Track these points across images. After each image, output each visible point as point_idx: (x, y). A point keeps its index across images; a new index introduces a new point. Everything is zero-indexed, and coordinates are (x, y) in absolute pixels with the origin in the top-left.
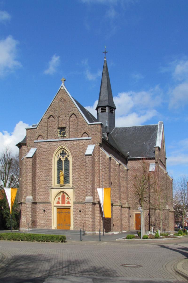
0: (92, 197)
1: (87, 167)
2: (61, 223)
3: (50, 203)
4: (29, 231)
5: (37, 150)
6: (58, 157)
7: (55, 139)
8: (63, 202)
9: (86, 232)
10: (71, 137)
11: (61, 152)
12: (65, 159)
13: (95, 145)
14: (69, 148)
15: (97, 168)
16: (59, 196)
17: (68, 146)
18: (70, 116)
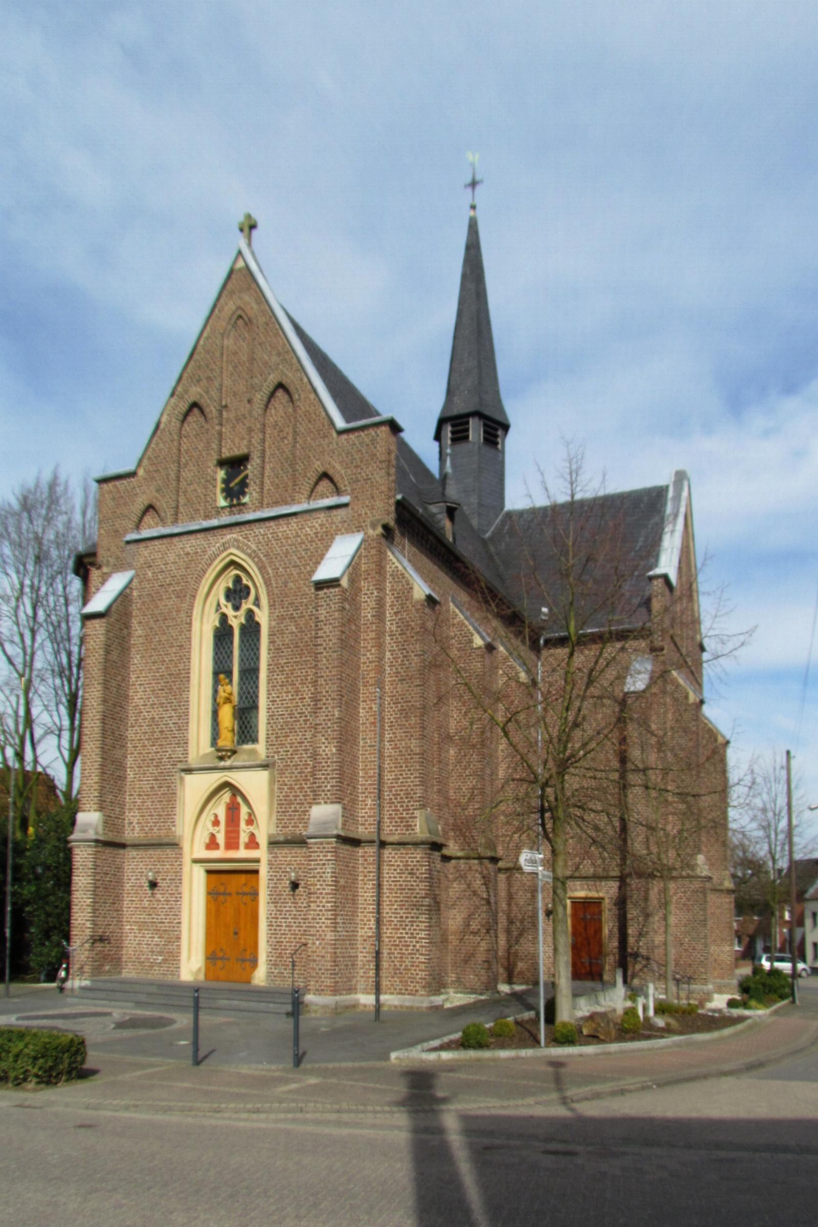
0: (336, 808)
1: (320, 649)
2: (222, 950)
3: (175, 845)
4: (76, 993)
5: (135, 580)
6: (217, 610)
7: (207, 517)
8: (232, 844)
9: (309, 998)
10: (268, 505)
11: (231, 585)
12: (243, 621)
13: (366, 533)
14: (256, 559)
15: (367, 656)
16: (215, 812)
17: (254, 551)
18: (265, 399)
